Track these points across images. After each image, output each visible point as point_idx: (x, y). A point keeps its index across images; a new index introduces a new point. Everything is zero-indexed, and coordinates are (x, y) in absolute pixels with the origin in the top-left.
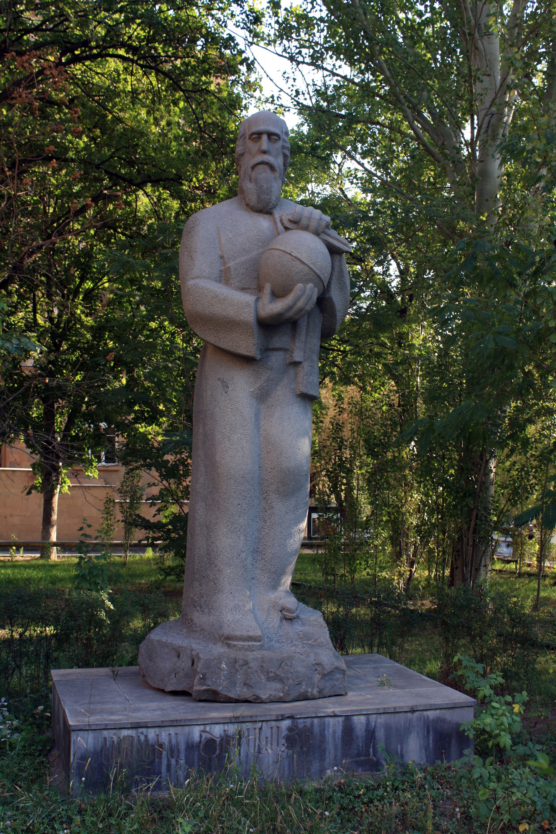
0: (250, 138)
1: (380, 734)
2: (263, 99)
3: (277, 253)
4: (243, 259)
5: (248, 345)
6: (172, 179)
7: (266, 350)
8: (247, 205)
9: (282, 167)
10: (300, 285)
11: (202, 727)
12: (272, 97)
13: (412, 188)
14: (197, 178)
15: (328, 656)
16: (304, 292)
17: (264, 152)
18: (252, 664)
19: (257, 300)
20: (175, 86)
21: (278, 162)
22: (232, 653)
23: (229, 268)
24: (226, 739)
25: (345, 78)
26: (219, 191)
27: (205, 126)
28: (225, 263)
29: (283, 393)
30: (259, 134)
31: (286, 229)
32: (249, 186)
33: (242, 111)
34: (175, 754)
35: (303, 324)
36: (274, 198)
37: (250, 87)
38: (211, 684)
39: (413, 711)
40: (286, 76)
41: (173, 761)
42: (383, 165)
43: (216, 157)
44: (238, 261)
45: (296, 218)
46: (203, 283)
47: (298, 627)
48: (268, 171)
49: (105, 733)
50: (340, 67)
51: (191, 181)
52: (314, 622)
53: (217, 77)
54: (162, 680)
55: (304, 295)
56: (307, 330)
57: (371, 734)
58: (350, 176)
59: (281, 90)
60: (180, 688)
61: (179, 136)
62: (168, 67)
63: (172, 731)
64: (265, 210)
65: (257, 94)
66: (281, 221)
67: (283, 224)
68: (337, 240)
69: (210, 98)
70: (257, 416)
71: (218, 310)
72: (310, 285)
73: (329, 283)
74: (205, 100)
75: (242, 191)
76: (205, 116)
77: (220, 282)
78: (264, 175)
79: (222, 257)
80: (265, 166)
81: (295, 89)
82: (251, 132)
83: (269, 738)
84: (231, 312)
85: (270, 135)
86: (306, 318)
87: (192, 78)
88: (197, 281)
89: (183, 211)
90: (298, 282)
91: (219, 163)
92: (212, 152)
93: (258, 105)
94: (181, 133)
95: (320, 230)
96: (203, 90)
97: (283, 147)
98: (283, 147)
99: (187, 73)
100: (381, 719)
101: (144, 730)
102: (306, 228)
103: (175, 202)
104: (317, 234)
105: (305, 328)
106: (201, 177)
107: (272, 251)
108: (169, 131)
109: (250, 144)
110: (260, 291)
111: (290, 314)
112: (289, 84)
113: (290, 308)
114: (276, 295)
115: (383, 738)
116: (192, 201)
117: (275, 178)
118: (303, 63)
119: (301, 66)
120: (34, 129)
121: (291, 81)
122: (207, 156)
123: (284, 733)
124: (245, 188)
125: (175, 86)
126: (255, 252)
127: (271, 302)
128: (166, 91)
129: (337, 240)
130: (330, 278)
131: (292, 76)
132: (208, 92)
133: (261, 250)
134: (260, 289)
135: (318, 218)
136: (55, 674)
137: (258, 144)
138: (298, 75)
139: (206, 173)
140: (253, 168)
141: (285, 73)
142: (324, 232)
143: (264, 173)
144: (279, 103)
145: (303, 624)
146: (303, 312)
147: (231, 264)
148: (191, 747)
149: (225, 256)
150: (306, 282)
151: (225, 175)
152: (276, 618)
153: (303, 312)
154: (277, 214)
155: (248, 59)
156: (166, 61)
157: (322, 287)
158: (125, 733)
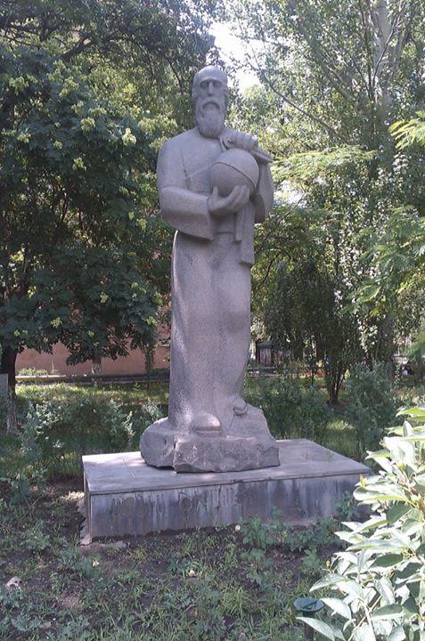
1: (303, 492)
5: (203, 231)
7: (217, 234)
8: (201, 133)
11: (180, 491)
15: (266, 438)
17: (210, 95)
18: (213, 446)
22: (202, 439)
24: (196, 499)
29: (230, 263)
34: (162, 510)
38: (186, 460)
39: (324, 476)
41: (161, 514)
46: (171, 189)
47: (246, 420)
48: (215, 109)
49: (114, 496)
52: (256, 415)
54: (154, 460)
55: (240, 193)
57: (296, 491)
60: (165, 465)
63: (159, 493)
70: (212, 278)
71: (182, 208)
83: (112, 478)
90: (236, 185)
100: (303, 482)
101: (140, 493)
102: (241, 147)
104: (249, 151)
109: (202, 90)
113: (230, 204)
115: (305, 496)
120: (339, 10)
123: (236, 492)
136: (86, 459)
145: (250, 418)
147: (191, 176)
148: (173, 504)
149: (187, 170)
152: (231, 414)
158: (127, 495)
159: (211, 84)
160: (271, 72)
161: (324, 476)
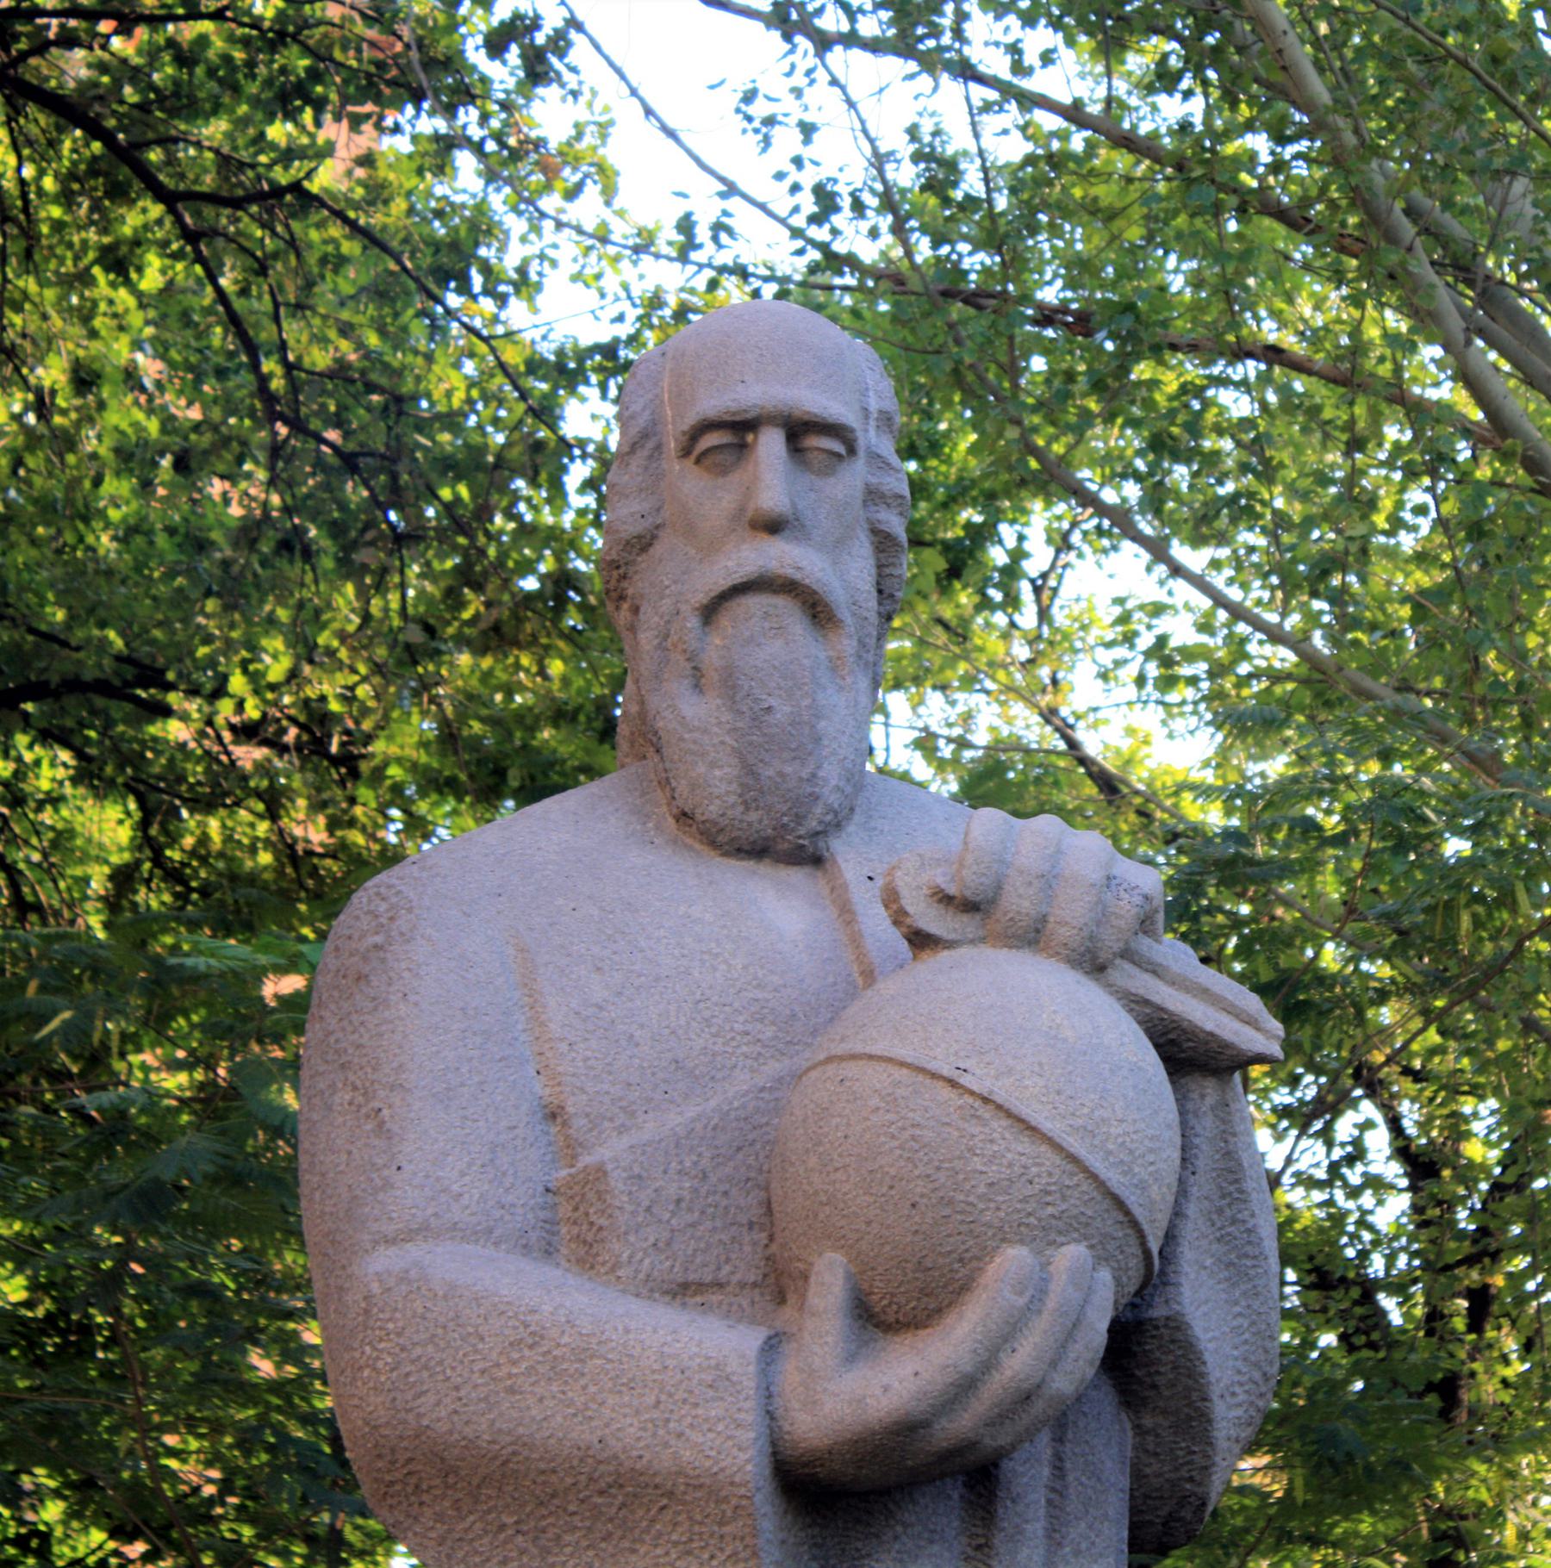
0: (686, 452)
2: (621, 231)
3: (877, 1077)
4: (676, 1119)
6: (102, 687)
9: (871, 603)
10: (1014, 1258)
12: (686, 225)
13: (1473, 695)
14: (256, 681)
16: (1042, 1291)
17: (773, 526)
19: (772, 1347)
20: (122, 169)
21: (847, 576)
23: (601, 1171)
25: (1074, 113)
26: (379, 747)
27: (294, 387)
28: (571, 1149)
30: (742, 428)
31: (921, 941)
32: (687, 712)
33: (502, 300)
35: (1029, 1477)
36: (831, 773)
37: (550, 171)
40: (759, 109)
42: (1305, 576)
43: (362, 556)
44: (649, 1129)
45: (971, 882)
46: (445, 1263)
50: (1047, 58)
51: (220, 691)
53: (356, 122)
55: (1033, 1315)
56: (1056, 1505)
58: (1121, 648)
59: (731, 190)
61: (144, 443)
62: (75, 67)
64: (786, 840)
65: (588, 209)
66: (891, 898)
67: (899, 917)
68: (1205, 994)
69: (318, 234)
71: (549, 1417)
72: (1071, 1254)
73: (1170, 1237)
74: (292, 243)
75: (650, 741)
76: (293, 330)
77: (549, 1252)
78: (773, 649)
79: (553, 1115)
80: (781, 602)
81: (808, 178)
82: (691, 419)
84: (625, 1428)
85: (799, 431)
86: (1044, 1438)
87: (215, 130)
88: (415, 1251)
89: (158, 859)
91: (380, 587)
92: (336, 530)
93: (593, 265)
94: (153, 426)
95: (1110, 941)
96: (278, 192)
97: (873, 496)
98: (873, 496)
99: (181, 102)
102: (1031, 936)
103: (113, 812)
104: (1094, 964)
105: (1037, 1497)
106: (276, 670)
107: (851, 1069)
108: (87, 419)
109: (689, 482)
110: (781, 1298)
111: (963, 1423)
112: (779, 157)
113: (966, 1386)
114: (877, 1318)
116: (205, 804)
117: (835, 666)
118: (851, 39)
119: (837, 55)
121: (787, 140)
122: (308, 554)
124: (665, 723)
125: (122, 169)
126: (742, 1081)
127: (851, 1359)
128: (66, 198)
129: (1205, 994)
130: (1178, 1213)
131: (790, 109)
132: (304, 199)
133: (774, 1068)
134: (779, 1284)
135: (1097, 876)
137: (736, 478)
138: (823, 103)
139: (306, 651)
140: (711, 611)
141: (749, 97)
142: (1128, 954)
143: (770, 640)
144: (724, 258)
146: (1038, 1407)
147: (610, 1150)
150: (1046, 1235)
151: (412, 655)
153: (1038, 1407)
154: (851, 857)
155: (536, 24)
156: (68, 41)
157: (1135, 1264)
159: (771, 443)
160: (1346, 629)
161: (986, 1100)
